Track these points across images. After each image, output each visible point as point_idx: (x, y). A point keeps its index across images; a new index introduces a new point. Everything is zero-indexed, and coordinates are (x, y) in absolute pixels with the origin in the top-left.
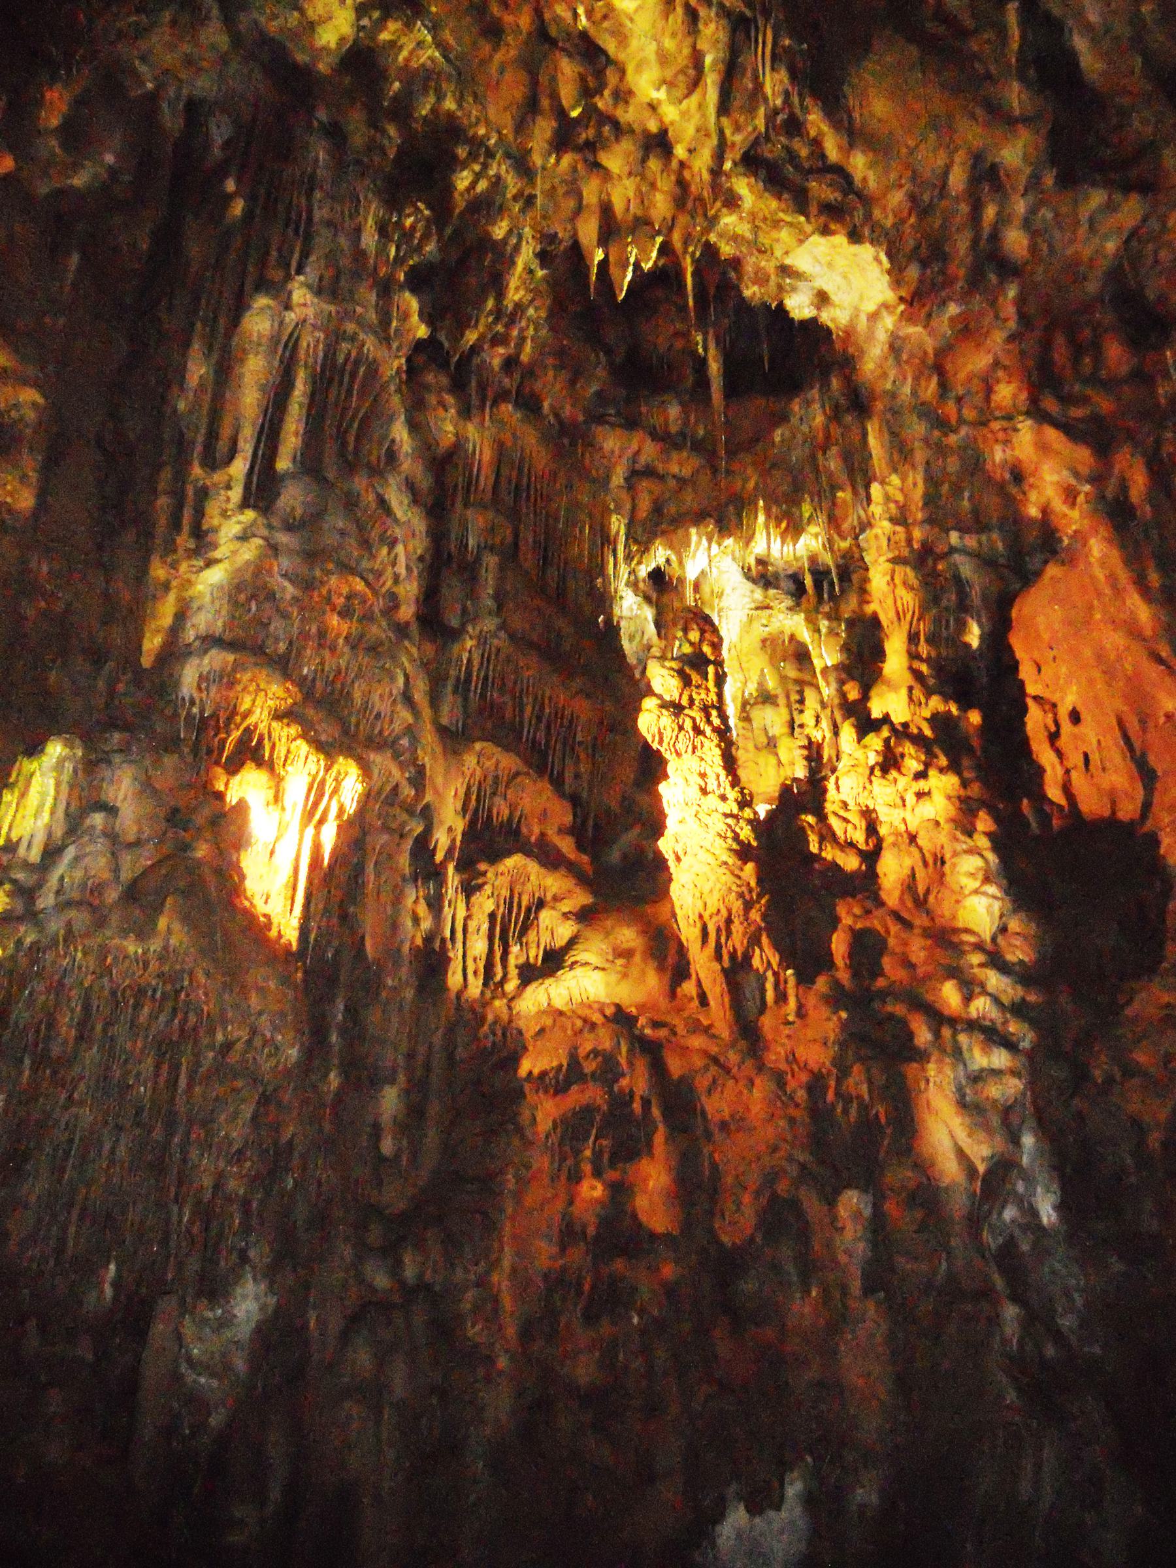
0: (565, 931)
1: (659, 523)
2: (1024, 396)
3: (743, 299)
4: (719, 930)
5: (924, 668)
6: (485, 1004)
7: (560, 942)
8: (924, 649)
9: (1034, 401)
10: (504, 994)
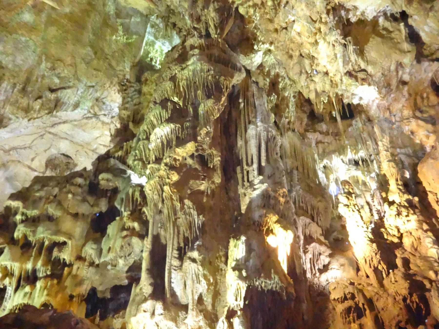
0: (327, 260)
1: (325, 154)
2: (411, 112)
4: (370, 260)
5: (401, 187)
6: (313, 280)
7: (326, 263)
8: (400, 183)
9: (414, 114)
10: (316, 277)
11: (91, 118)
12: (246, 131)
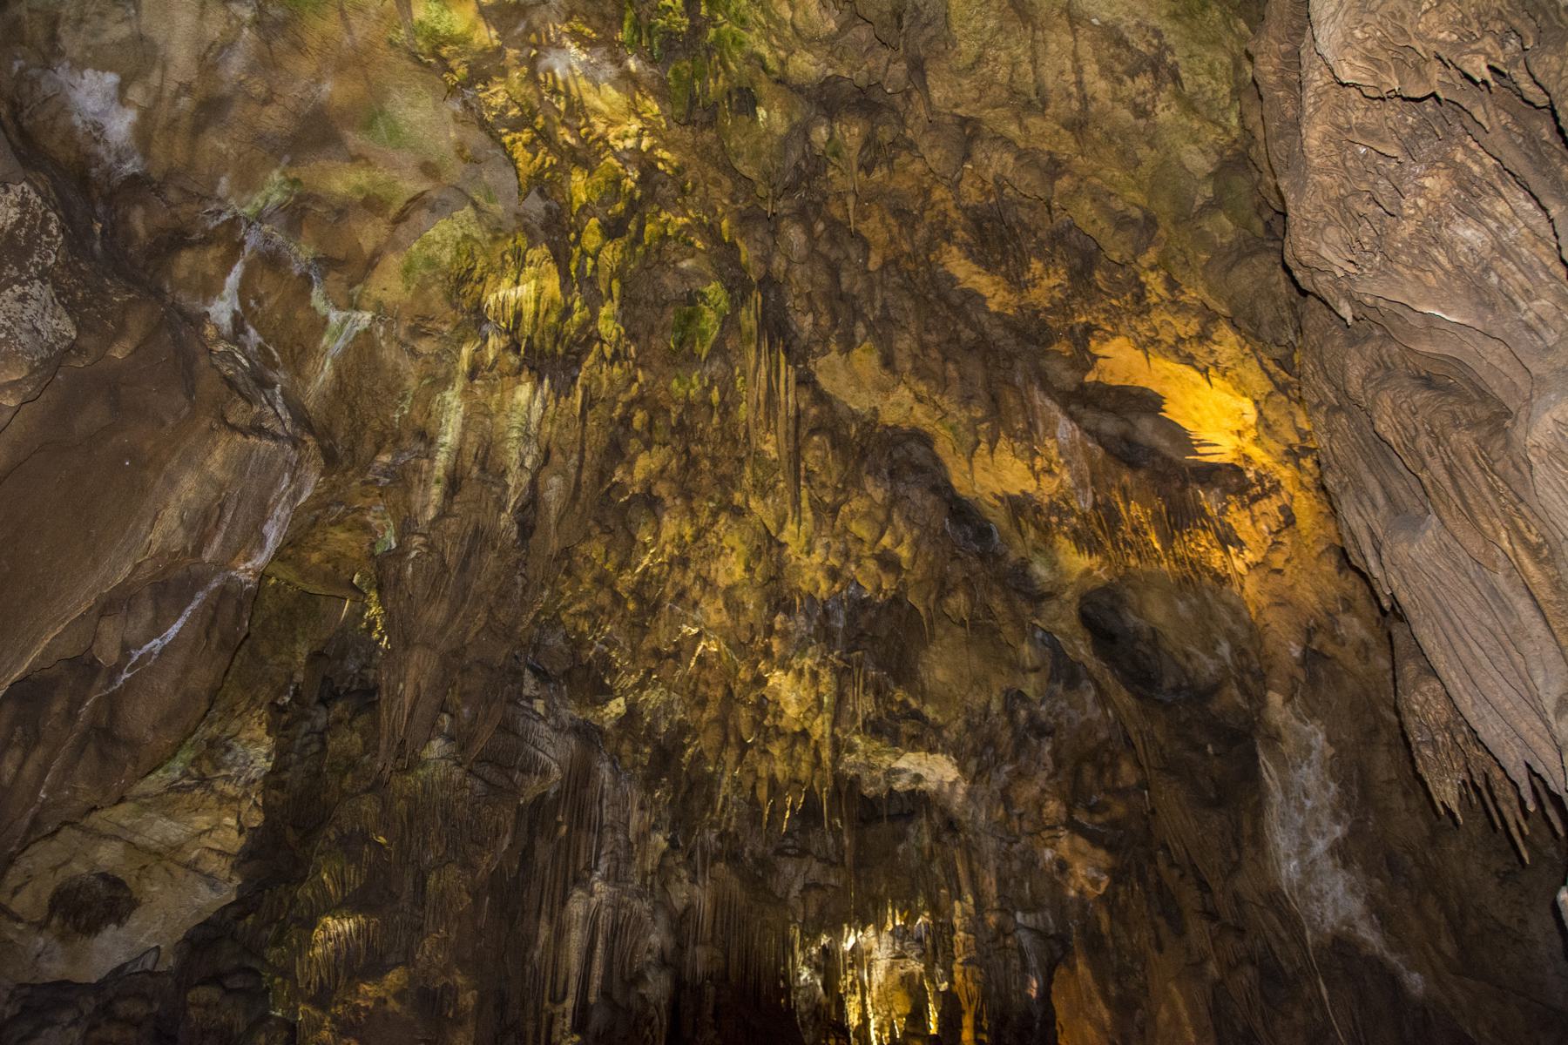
3: (862, 796)
9: (1070, 814)
11: (189, 789)
12: (564, 903)
